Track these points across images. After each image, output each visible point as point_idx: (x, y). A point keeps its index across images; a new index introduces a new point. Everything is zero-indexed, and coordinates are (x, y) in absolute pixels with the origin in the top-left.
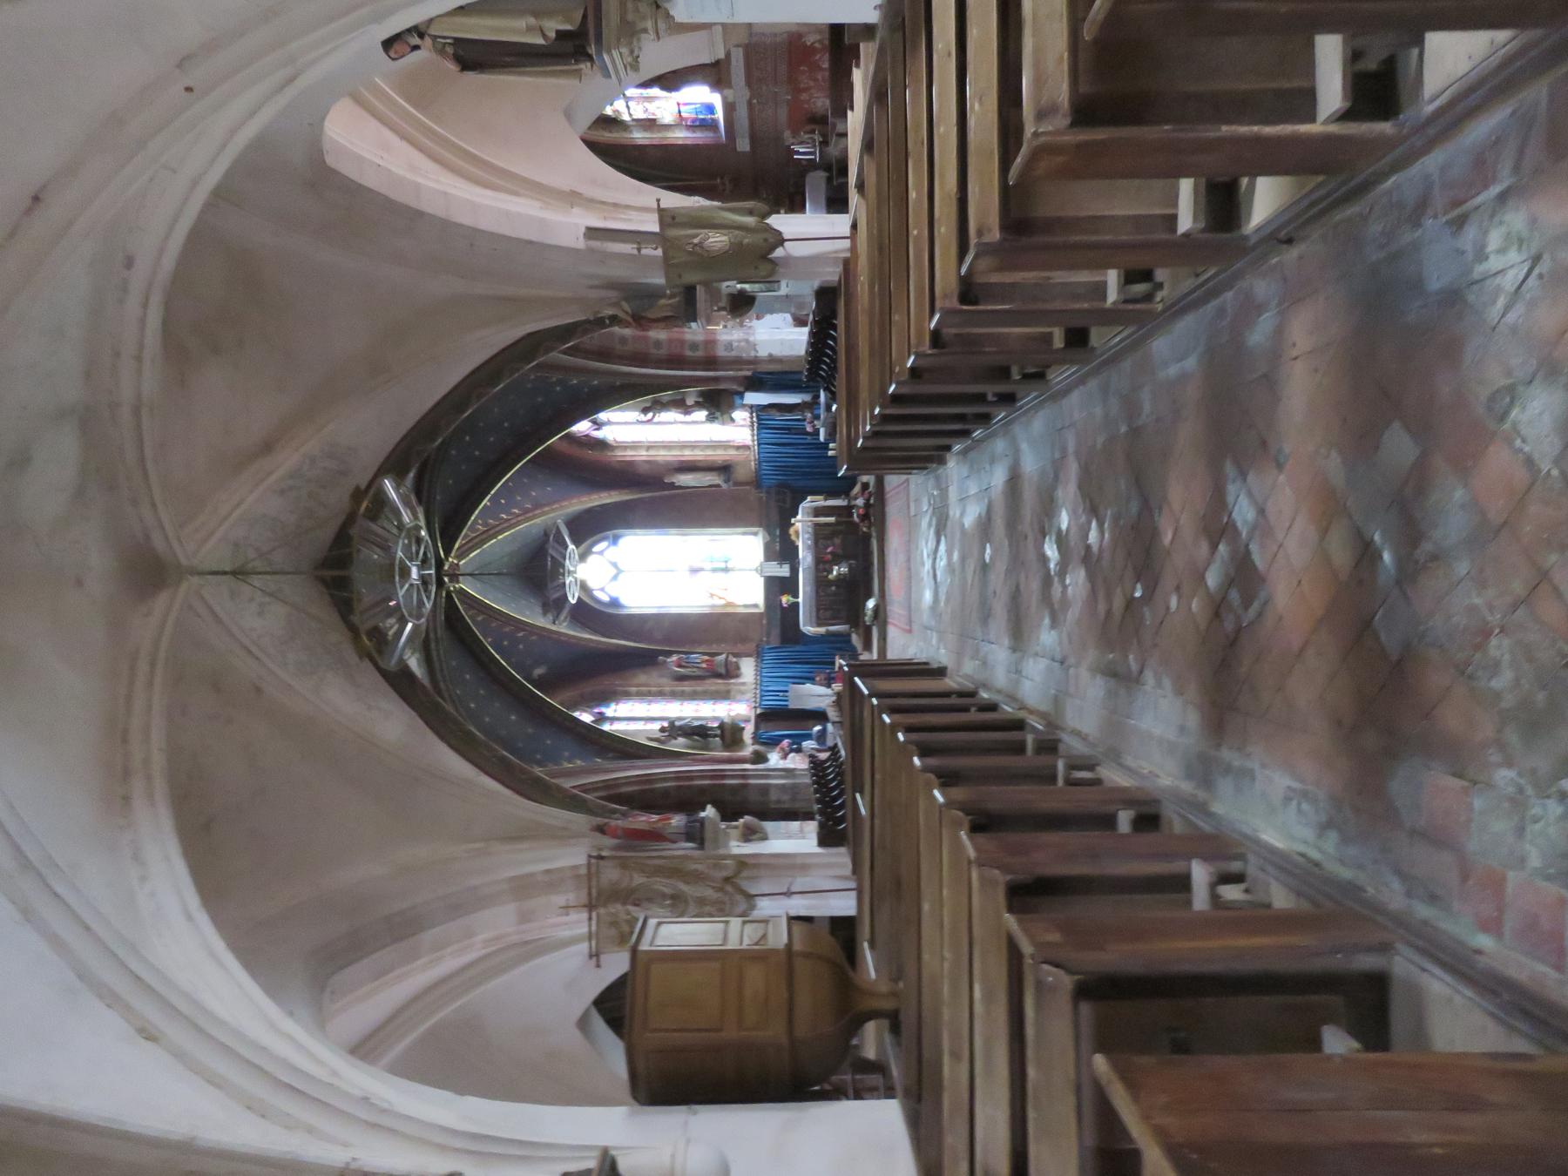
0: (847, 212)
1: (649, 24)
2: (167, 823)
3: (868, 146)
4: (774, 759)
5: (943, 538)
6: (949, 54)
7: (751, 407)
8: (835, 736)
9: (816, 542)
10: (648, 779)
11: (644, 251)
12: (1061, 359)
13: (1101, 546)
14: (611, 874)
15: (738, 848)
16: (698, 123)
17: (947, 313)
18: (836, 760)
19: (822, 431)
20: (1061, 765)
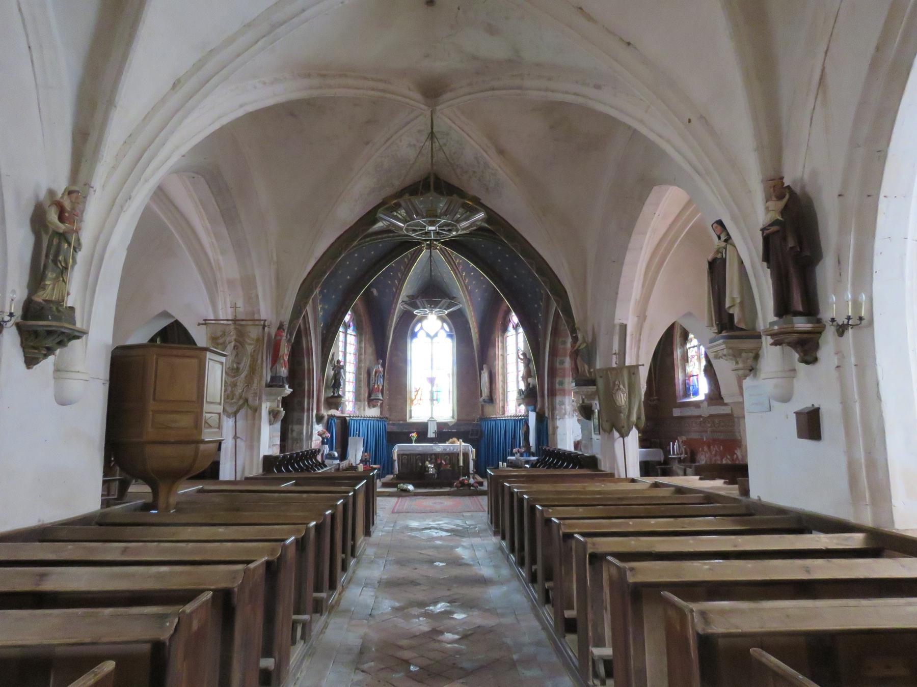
0: (641, 476)
1: (741, 365)
2: (294, 96)
3: (680, 490)
4: (318, 428)
5: (449, 534)
6: (735, 546)
7: (527, 416)
8: (332, 465)
9: (448, 454)
10: (309, 354)
11: (614, 357)
12: (558, 614)
13: (443, 642)
14: (254, 333)
15: (265, 407)
16: (687, 386)
17: (584, 545)
18: (316, 466)
19: (513, 458)
20: (305, 617)
